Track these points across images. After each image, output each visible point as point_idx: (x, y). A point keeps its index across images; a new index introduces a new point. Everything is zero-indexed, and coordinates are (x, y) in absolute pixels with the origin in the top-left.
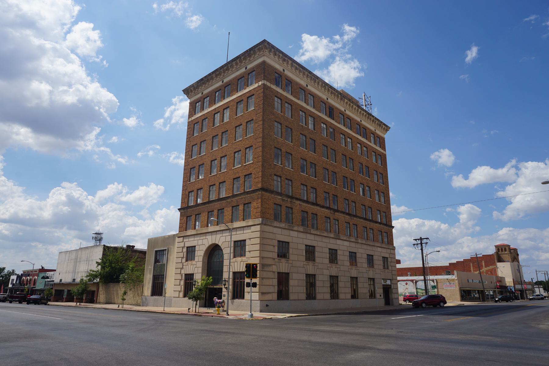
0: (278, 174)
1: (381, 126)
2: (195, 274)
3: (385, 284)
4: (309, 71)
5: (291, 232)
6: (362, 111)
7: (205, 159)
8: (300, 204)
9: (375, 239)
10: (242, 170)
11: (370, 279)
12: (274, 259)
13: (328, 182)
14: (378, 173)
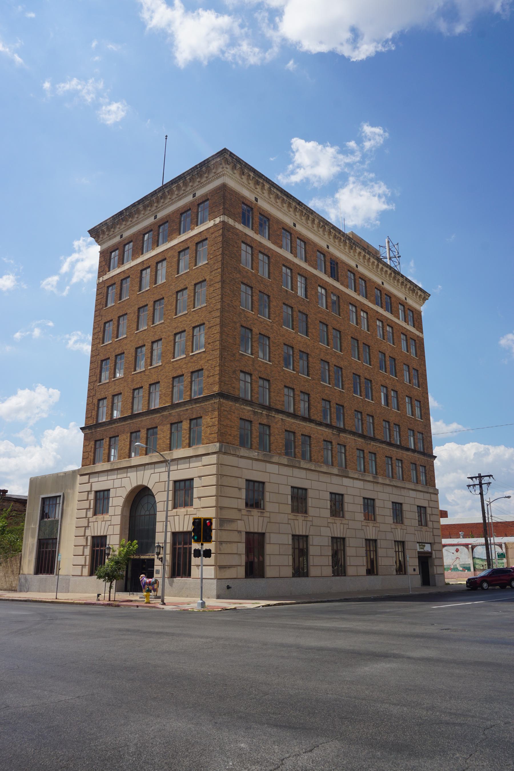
0: (246, 369)
3: (422, 550)
5: (268, 465)
6: (384, 267)
8: (282, 419)
9: (405, 477)
12: (240, 510)
13: (329, 384)
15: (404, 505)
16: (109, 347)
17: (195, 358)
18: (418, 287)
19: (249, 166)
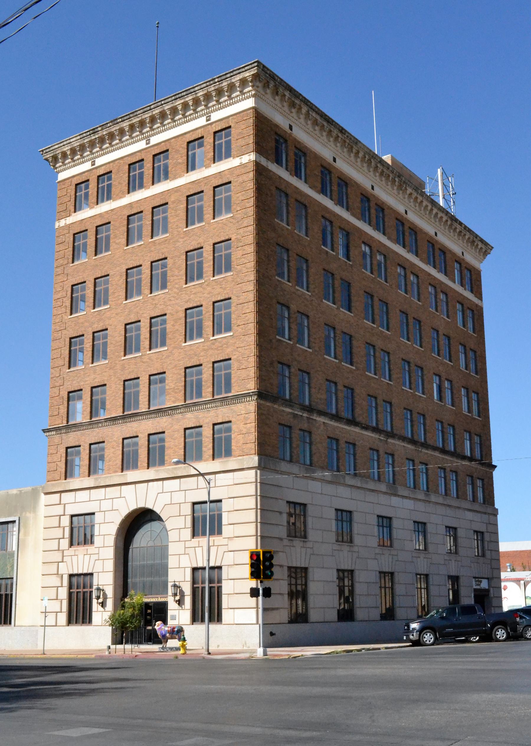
0: (284, 360)
1: (475, 244)
2: (95, 575)
3: (478, 587)
4: (341, 127)
5: (311, 482)
6: (439, 212)
7: (110, 318)
8: (324, 422)
9: (460, 493)
10: (206, 350)
11: (450, 577)
12: (281, 539)
13: (375, 374)
14: (468, 349)
15: (458, 529)
16: (81, 321)
17: (217, 344)
18: (478, 238)
19: (285, 82)
